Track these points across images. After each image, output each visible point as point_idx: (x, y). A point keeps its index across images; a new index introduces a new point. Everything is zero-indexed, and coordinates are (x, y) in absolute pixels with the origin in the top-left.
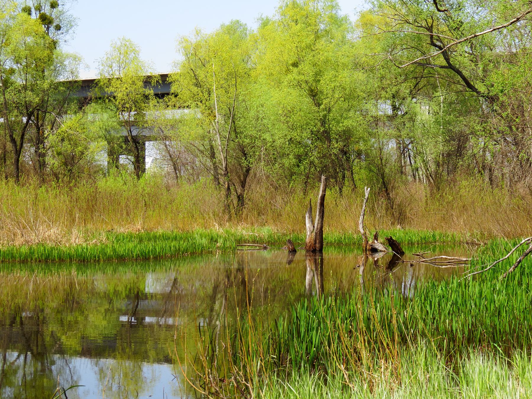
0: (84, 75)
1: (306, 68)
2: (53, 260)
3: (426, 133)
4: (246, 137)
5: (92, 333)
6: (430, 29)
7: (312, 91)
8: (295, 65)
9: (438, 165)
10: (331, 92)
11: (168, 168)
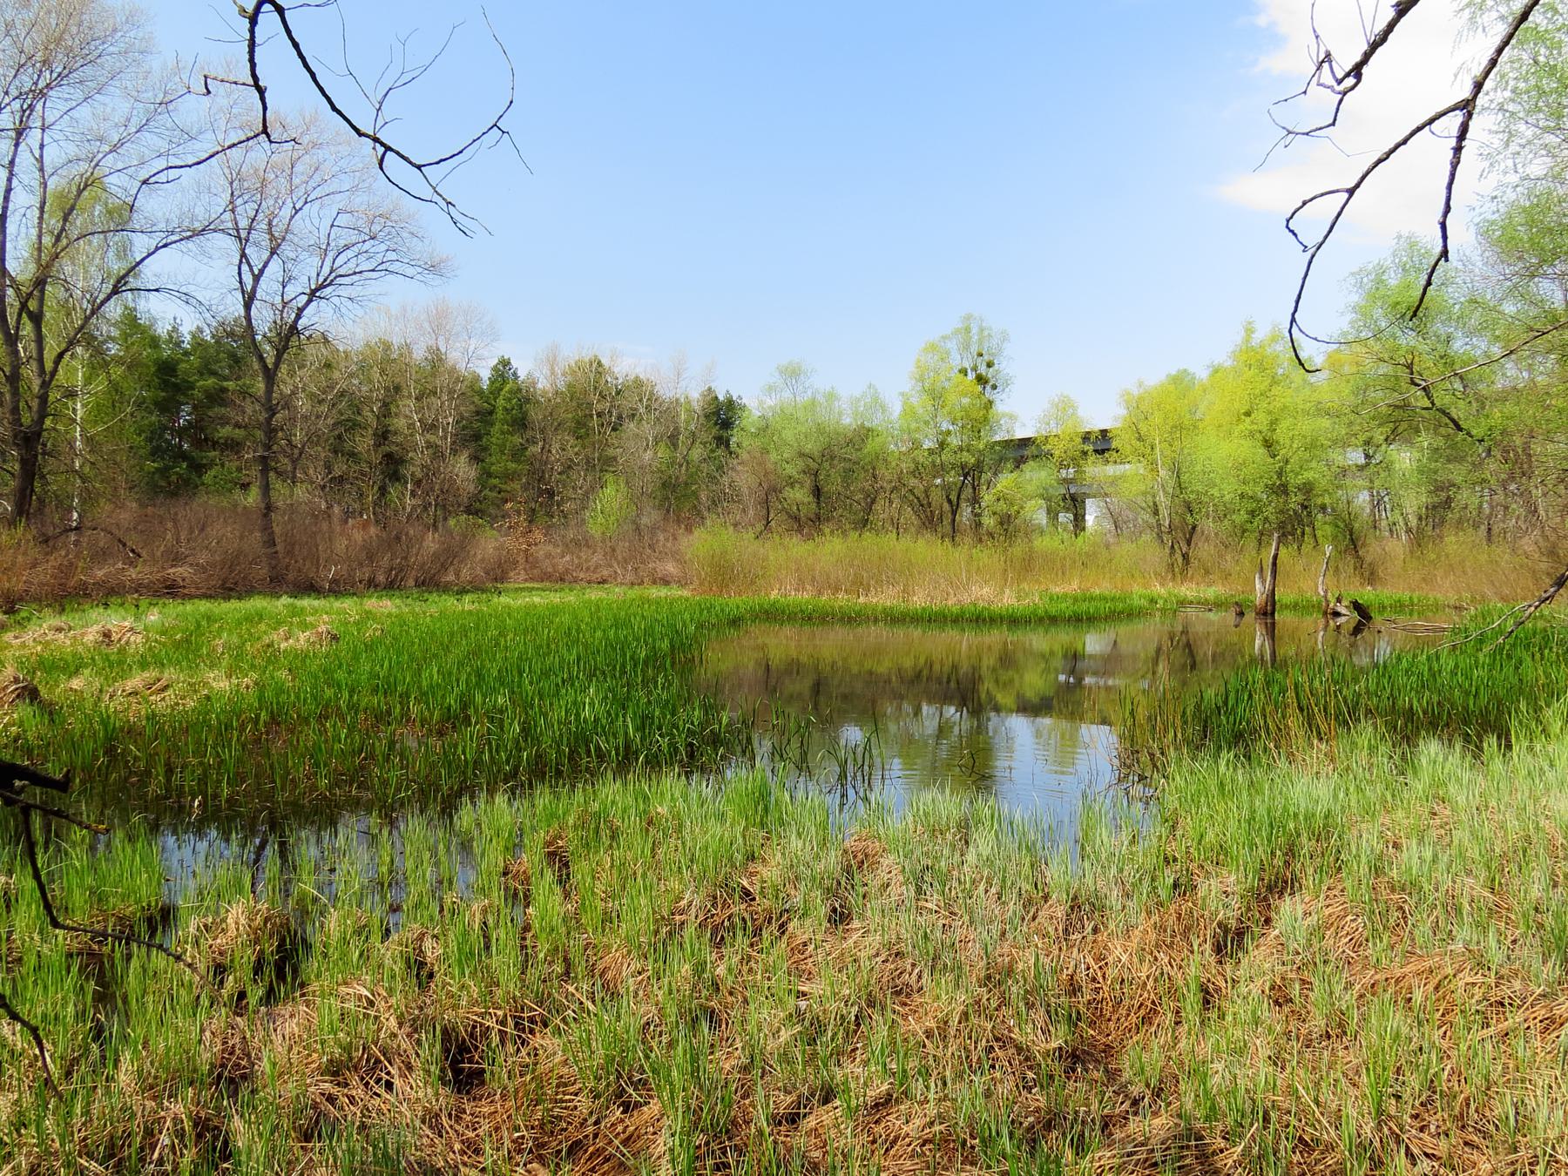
0: (1020, 434)
1: (1261, 418)
2: (984, 620)
3: (1405, 484)
4: (1192, 492)
5: (1030, 694)
6: (1410, 367)
7: (1266, 441)
8: (1248, 414)
9: (1420, 519)
10: (1288, 442)
11: (1109, 526)
